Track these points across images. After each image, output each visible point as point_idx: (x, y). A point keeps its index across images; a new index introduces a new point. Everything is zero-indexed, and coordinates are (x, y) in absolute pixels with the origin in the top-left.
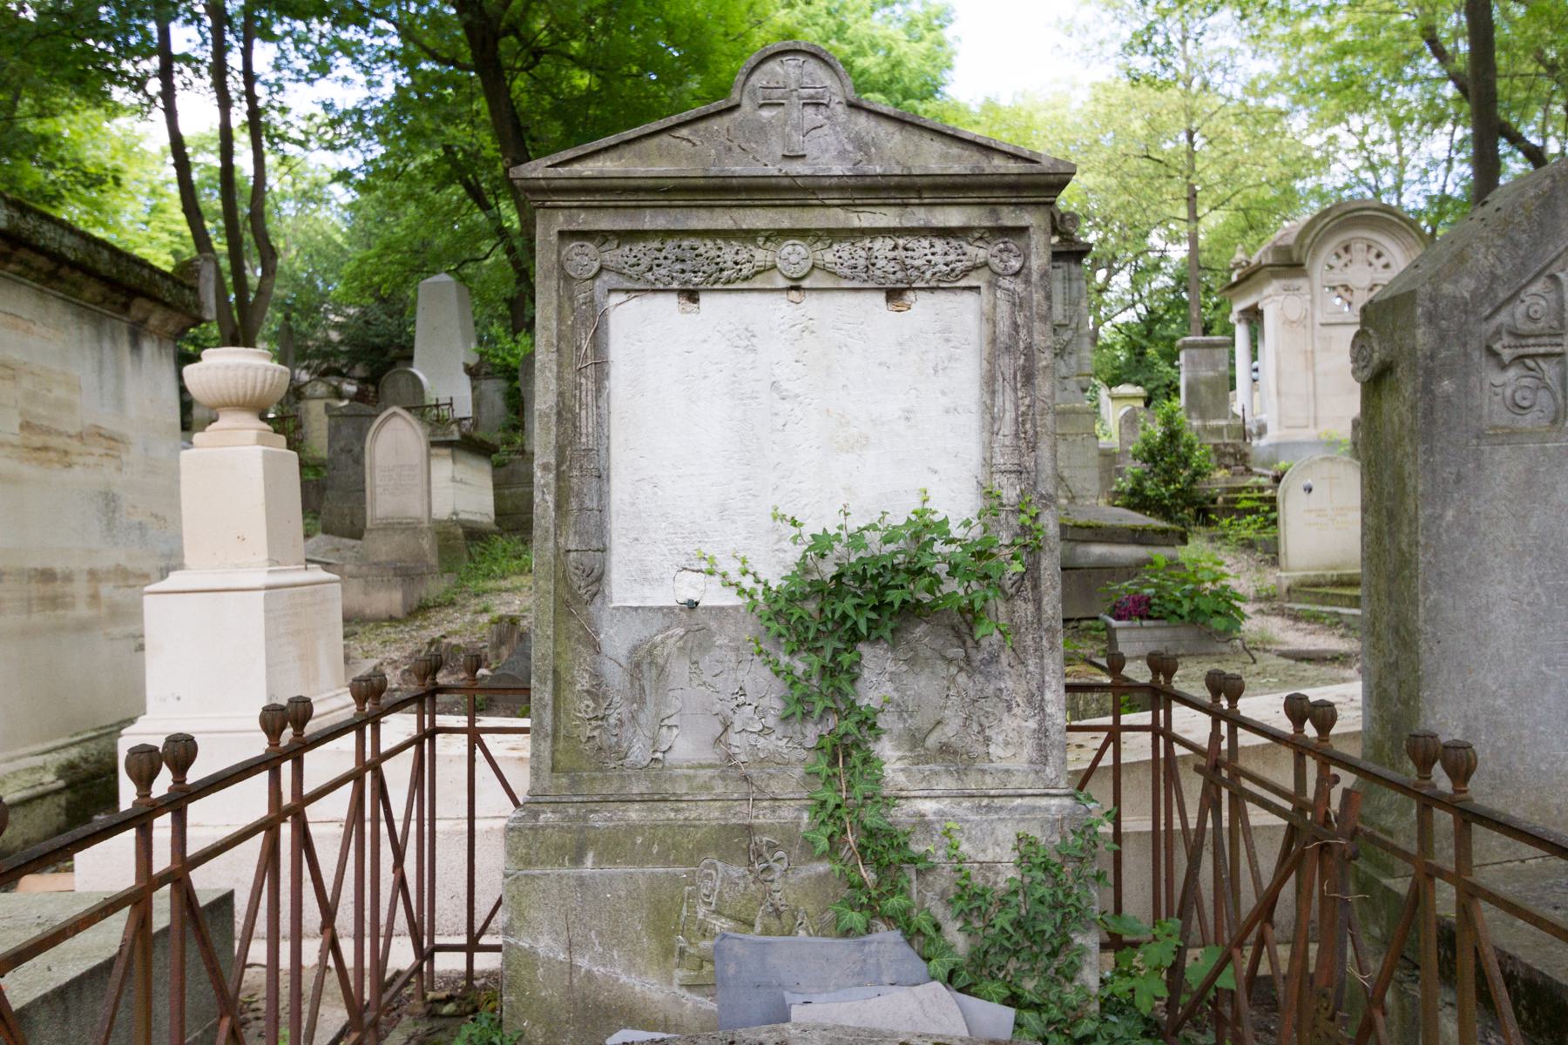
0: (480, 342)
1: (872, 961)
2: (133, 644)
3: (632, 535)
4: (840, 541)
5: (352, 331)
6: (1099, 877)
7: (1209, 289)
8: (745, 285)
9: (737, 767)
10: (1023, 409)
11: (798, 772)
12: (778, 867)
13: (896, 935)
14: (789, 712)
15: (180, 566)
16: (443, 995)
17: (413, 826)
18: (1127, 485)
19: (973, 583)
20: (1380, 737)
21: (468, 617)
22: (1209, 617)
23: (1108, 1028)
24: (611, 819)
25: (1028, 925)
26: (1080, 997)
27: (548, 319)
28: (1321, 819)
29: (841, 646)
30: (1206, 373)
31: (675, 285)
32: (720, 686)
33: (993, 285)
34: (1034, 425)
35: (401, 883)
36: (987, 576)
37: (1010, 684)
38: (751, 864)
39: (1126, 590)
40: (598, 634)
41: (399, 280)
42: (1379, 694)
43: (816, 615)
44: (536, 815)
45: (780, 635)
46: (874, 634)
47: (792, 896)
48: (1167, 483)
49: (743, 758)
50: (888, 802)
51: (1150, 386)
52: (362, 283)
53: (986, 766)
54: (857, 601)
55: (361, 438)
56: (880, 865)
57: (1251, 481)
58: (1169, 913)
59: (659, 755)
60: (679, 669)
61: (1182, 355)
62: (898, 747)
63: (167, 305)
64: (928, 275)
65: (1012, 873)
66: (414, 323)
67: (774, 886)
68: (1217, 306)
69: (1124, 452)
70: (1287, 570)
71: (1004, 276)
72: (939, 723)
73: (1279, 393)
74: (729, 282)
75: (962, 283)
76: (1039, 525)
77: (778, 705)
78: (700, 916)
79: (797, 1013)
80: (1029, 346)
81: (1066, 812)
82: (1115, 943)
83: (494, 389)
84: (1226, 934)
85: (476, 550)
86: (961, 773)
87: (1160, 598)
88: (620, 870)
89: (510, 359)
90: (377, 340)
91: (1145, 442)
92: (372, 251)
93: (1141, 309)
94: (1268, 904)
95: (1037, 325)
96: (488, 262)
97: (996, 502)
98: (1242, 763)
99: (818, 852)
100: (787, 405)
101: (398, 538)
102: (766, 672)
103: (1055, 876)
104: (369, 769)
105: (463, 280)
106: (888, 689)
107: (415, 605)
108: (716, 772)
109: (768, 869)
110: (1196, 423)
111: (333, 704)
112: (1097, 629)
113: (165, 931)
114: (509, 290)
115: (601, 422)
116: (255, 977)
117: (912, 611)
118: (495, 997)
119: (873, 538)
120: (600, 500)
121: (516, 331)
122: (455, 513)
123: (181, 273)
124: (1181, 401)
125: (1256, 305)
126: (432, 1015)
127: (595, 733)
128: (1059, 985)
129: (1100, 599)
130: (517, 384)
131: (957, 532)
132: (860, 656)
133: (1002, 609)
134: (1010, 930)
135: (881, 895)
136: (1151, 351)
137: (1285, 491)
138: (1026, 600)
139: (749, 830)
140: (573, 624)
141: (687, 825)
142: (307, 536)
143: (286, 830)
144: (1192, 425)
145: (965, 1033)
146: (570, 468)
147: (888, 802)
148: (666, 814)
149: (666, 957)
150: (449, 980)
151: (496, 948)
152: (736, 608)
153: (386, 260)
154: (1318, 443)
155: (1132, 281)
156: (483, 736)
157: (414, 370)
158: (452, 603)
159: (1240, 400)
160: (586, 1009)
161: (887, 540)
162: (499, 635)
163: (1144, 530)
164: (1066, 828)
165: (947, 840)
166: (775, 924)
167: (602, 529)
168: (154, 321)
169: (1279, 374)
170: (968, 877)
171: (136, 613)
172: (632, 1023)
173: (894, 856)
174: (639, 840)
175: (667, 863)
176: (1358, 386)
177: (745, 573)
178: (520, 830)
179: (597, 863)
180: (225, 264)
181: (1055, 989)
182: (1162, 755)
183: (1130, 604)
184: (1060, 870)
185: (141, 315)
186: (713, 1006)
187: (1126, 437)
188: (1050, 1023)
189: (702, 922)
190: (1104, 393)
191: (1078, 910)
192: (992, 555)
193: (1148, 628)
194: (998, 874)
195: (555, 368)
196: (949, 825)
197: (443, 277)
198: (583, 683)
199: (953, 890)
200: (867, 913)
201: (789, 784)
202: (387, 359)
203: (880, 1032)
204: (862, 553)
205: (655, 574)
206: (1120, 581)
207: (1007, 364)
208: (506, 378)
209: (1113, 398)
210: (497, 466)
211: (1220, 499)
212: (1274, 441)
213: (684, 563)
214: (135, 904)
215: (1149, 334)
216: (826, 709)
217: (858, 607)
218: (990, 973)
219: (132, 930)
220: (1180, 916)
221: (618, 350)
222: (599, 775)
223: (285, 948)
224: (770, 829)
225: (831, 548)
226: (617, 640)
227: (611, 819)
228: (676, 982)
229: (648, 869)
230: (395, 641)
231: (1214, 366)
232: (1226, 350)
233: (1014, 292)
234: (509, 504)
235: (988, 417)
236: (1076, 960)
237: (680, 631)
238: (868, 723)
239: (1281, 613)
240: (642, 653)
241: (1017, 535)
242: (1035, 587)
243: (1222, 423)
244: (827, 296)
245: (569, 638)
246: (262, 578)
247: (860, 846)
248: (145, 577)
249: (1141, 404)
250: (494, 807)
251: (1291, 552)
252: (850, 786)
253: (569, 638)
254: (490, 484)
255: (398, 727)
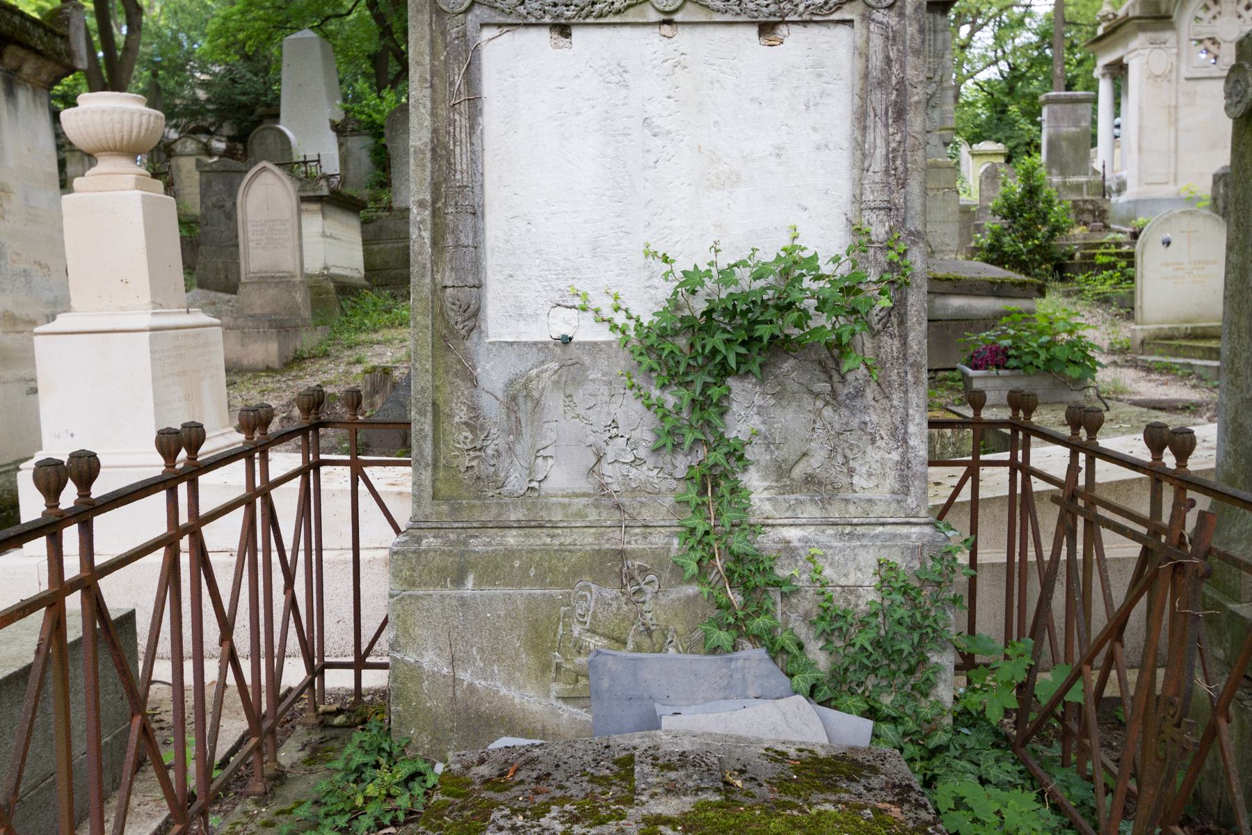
0: (345, 100)
1: (738, 676)
2: (24, 387)
3: (507, 272)
4: (711, 277)
5: (218, 89)
6: (956, 600)
7: (1073, 46)
8: (617, 19)
9: (610, 496)
10: (894, 145)
11: (669, 500)
12: (648, 589)
13: (761, 652)
14: (660, 443)
15: (68, 309)
16: (334, 707)
17: (301, 556)
18: (986, 241)
19: (840, 318)
20: (1233, 470)
21: (342, 368)
22: (1066, 365)
23: (961, 739)
24: (490, 544)
25: (887, 645)
26: (935, 711)
27: (421, 54)
28: (1175, 541)
29: (710, 380)
30: (1068, 129)
31: (547, 19)
32: (593, 419)
33: (866, 18)
34: (905, 162)
35: (292, 604)
36: (855, 311)
37: (875, 418)
38: (623, 586)
39: (984, 340)
40: (475, 368)
41: (263, 37)
42: (1234, 430)
43: (686, 350)
44: (418, 540)
45: (652, 370)
46: (743, 369)
47: (662, 616)
48: (1025, 239)
49: (615, 487)
50: (754, 529)
51: (1010, 144)
52: (227, 38)
53: (850, 496)
54: (727, 336)
55: (233, 194)
56: (746, 588)
57: (1109, 237)
58: (1021, 634)
59: (535, 484)
60: (554, 403)
61: (1045, 111)
62: (764, 478)
63: (39, 53)
64: (801, 8)
65: (872, 596)
66: (279, 81)
67: (645, 607)
68: (1080, 63)
69: (983, 209)
70: (1142, 324)
71: (877, 9)
72: (805, 454)
73: (1140, 149)
74: (601, 16)
75: (835, 16)
76: (907, 262)
77: (649, 437)
78: (576, 634)
79: (666, 722)
80: (902, 82)
81: (925, 540)
82: (967, 663)
83: (360, 145)
84: (1076, 650)
85: (347, 304)
86: (825, 502)
87: (1017, 348)
88: (499, 591)
89: (375, 116)
90: (244, 98)
91: (1005, 197)
92: (236, 7)
93: (1003, 66)
94: (1117, 627)
95: (910, 59)
96: (351, 17)
97: (865, 239)
98: (1098, 493)
99: (687, 576)
100: (658, 142)
101: (272, 292)
102: (638, 406)
103: (914, 599)
104: (257, 497)
105: (326, 36)
106: (756, 422)
107: (291, 355)
108: (591, 500)
109: (640, 591)
110: (1056, 180)
111: (222, 436)
112: (953, 380)
113: (77, 643)
114: (373, 46)
115: (475, 160)
116: (160, 694)
117: (780, 346)
118: (383, 710)
119: (743, 274)
120: (475, 237)
121: (380, 88)
122: (326, 268)
123: (51, 21)
124: (1043, 157)
125: (1121, 59)
126: (324, 725)
127: (474, 463)
128: (915, 699)
129: (961, 352)
130: (383, 141)
131: (826, 269)
132: (729, 390)
133: (868, 345)
134: (870, 648)
135: (748, 616)
136: (1013, 109)
137: (1144, 245)
138: (892, 336)
139: (621, 554)
140: (451, 358)
141: (562, 549)
142: (187, 291)
143: (185, 543)
144: (1052, 181)
145: (826, 741)
146: (446, 205)
147: (754, 529)
148: (542, 539)
149: (543, 672)
150: (337, 697)
151: (384, 666)
152: (609, 344)
153: (249, 17)
154: (1178, 200)
155: (996, 37)
156: (366, 470)
157: (281, 127)
158: (326, 355)
159: (1101, 156)
160: (469, 719)
161: (757, 277)
162: (373, 384)
163: (1003, 282)
164: (926, 554)
165: (810, 565)
166: (647, 643)
167: (477, 266)
168: (28, 69)
169: (1141, 129)
170: (830, 600)
171: (27, 357)
172: (511, 732)
173: (760, 580)
174: (517, 564)
175: (543, 585)
176: (1231, 121)
177: (617, 309)
178: (403, 553)
179: (478, 584)
180: (92, 22)
181: (911, 704)
182: (1019, 491)
183: (987, 354)
184: (919, 593)
185: (14, 64)
186: (589, 717)
187: (985, 193)
188: (905, 734)
189: (577, 640)
190: (964, 150)
191: (934, 631)
192: (861, 291)
193: (1003, 377)
194: (859, 597)
195: (429, 104)
196: (813, 551)
197: (307, 33)
198: (462, 415)
199: (815, 612)
200: (734, 632)
201: (659, 511)
202: (254, 118)
203: (746, 739)
204: (732, 289)
205: (529, 310)
206: (978, 331)
207: (879, 100)
208: (374, 136)
209: (973, 155)
210: (365, 222)
211: (1078, 255)
212: (1133, 198)
213: (557, 299)
214: (50, 607)
215: (1011, 91)
216: (696, 441)
217: (728, 342)
218: (850, 689)
219: (48, 630)
220: (1032, 636)
221: (491, 85)
222: (478, 502)
223: (188, 666)
224: (642, 554)
225: (702, 284)
226: (494, 375)
227: (490, 544)
228: (553, 694)
229: (526, 591)
230: (273, 390)
231: (1076, 122)
232: (1090, 105)
233: (887, 26)
234: (378, 260)
235: (858, 153)
236: (931, 676)
237: (554, 366)
238: (736, 454)
239: (1134, 365)
240: (518, 387)
241: (885, 272)
242: (902, 323)
243: (1083, 179)
244: (699, 30)
245: (447, 372)
246: (146, 320)
247: (728, 570)
248: (34, 323)
249: (1002, 160)
250: (378, 537)
251: (1145, 306)
252: (718, 514)
253: (447, 372)
254: (359, 240)
255: (284, 461)
